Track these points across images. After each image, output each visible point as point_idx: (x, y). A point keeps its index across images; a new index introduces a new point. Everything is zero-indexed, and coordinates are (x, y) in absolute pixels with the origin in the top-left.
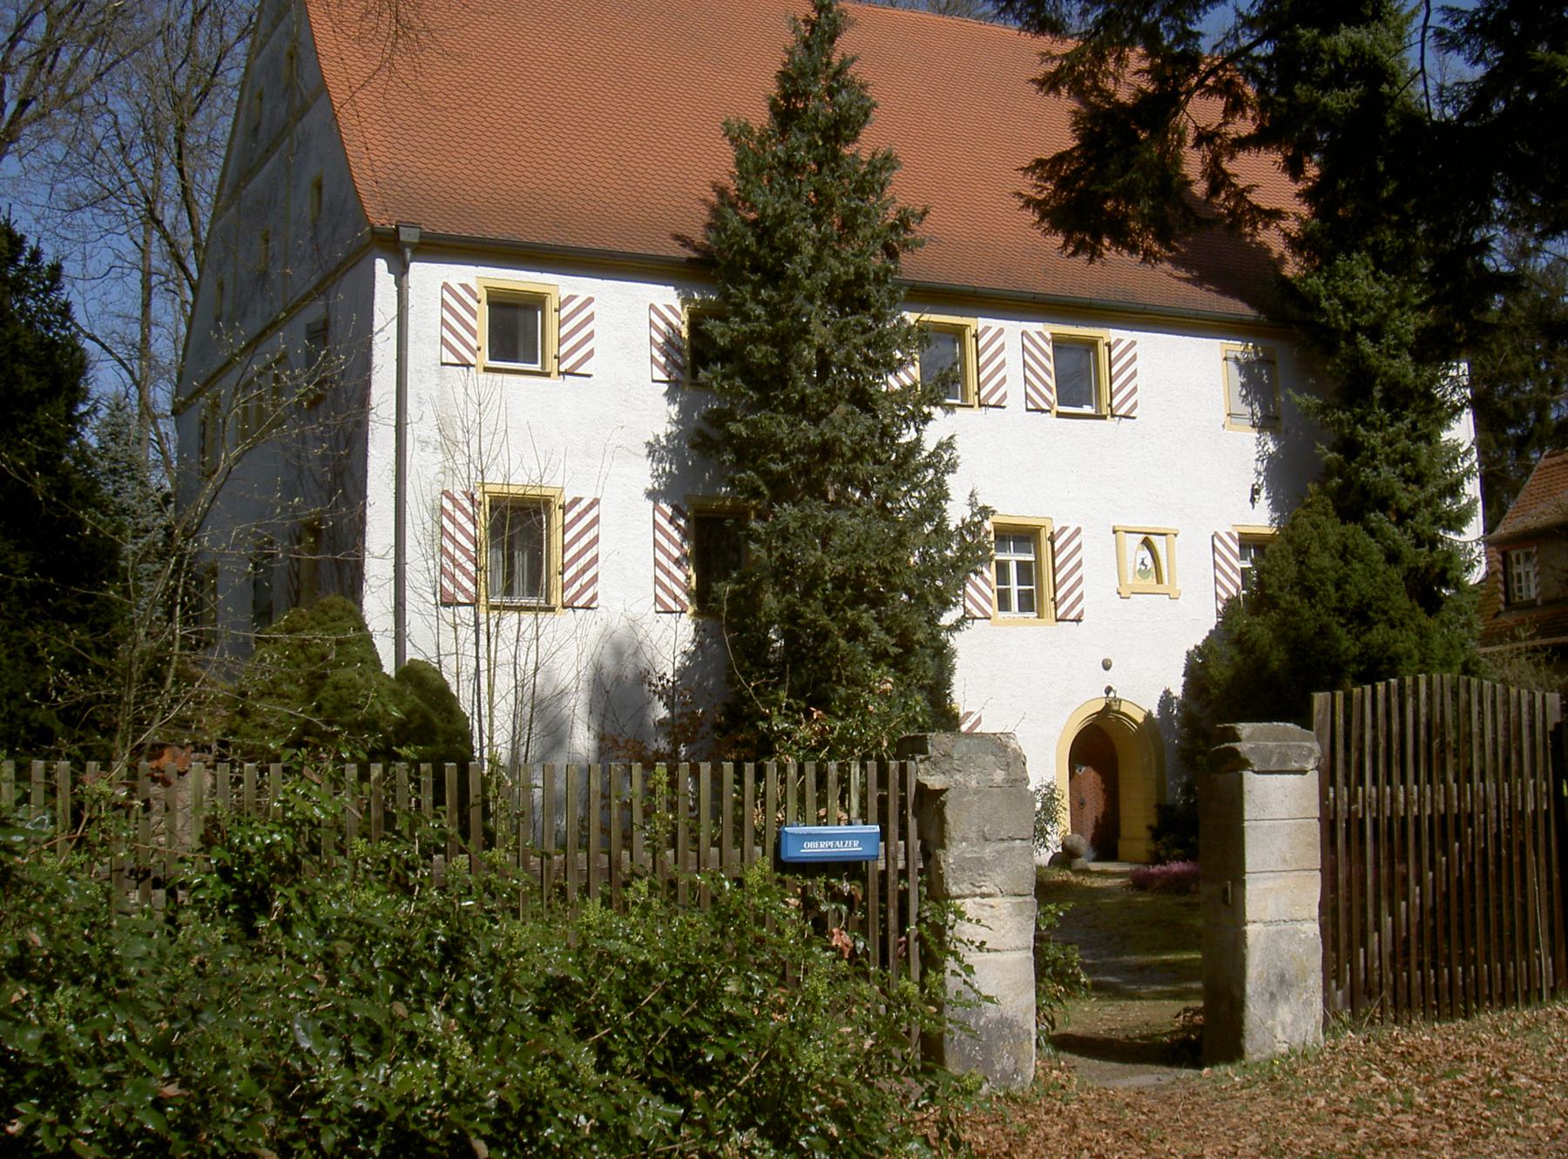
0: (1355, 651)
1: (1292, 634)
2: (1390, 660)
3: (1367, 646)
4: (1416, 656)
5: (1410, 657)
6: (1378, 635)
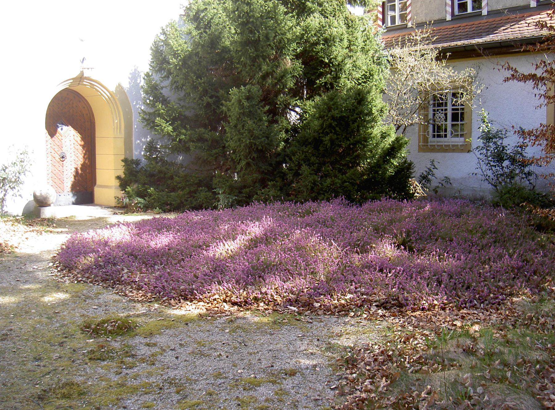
0: (298, 30)
1: (246, 8)
2: (326, 40)
3: (306, 29)
4: (346, 43)
5: (341, 40)
6: (314, 21)
